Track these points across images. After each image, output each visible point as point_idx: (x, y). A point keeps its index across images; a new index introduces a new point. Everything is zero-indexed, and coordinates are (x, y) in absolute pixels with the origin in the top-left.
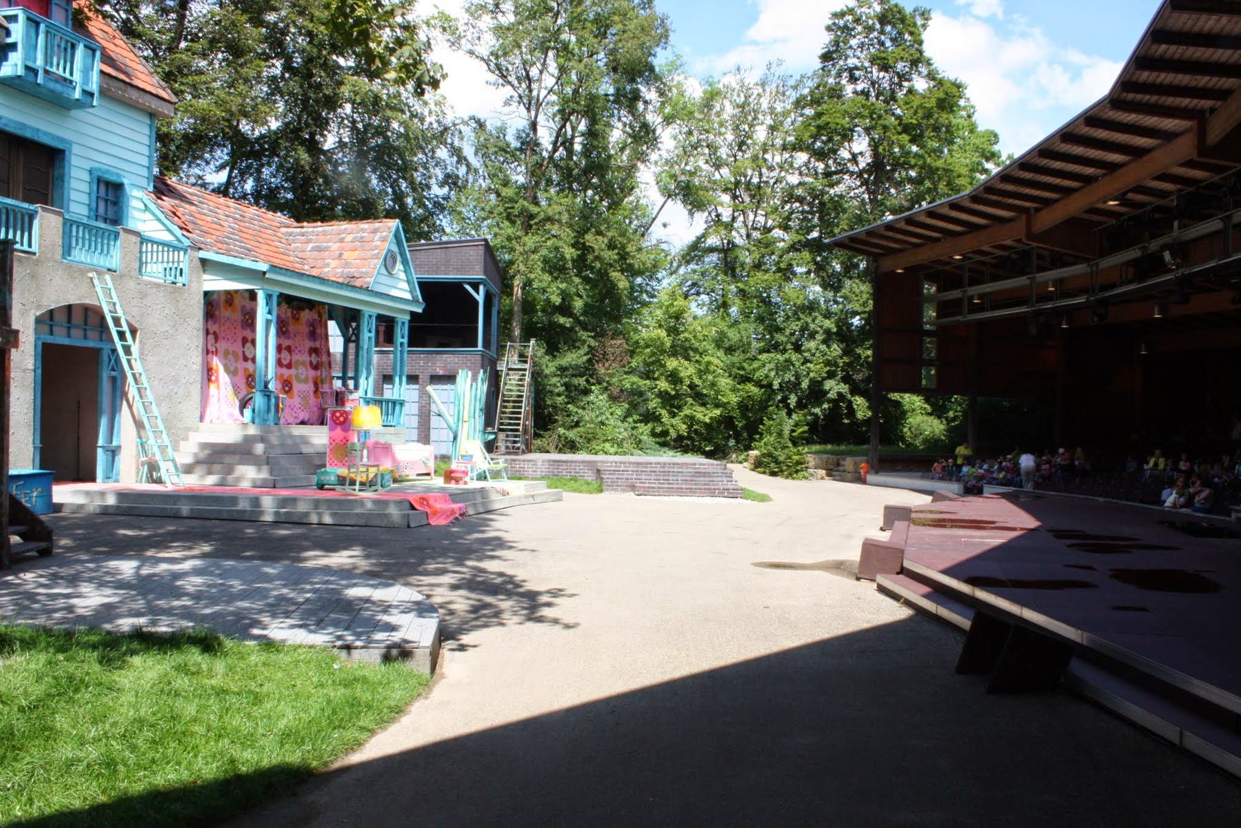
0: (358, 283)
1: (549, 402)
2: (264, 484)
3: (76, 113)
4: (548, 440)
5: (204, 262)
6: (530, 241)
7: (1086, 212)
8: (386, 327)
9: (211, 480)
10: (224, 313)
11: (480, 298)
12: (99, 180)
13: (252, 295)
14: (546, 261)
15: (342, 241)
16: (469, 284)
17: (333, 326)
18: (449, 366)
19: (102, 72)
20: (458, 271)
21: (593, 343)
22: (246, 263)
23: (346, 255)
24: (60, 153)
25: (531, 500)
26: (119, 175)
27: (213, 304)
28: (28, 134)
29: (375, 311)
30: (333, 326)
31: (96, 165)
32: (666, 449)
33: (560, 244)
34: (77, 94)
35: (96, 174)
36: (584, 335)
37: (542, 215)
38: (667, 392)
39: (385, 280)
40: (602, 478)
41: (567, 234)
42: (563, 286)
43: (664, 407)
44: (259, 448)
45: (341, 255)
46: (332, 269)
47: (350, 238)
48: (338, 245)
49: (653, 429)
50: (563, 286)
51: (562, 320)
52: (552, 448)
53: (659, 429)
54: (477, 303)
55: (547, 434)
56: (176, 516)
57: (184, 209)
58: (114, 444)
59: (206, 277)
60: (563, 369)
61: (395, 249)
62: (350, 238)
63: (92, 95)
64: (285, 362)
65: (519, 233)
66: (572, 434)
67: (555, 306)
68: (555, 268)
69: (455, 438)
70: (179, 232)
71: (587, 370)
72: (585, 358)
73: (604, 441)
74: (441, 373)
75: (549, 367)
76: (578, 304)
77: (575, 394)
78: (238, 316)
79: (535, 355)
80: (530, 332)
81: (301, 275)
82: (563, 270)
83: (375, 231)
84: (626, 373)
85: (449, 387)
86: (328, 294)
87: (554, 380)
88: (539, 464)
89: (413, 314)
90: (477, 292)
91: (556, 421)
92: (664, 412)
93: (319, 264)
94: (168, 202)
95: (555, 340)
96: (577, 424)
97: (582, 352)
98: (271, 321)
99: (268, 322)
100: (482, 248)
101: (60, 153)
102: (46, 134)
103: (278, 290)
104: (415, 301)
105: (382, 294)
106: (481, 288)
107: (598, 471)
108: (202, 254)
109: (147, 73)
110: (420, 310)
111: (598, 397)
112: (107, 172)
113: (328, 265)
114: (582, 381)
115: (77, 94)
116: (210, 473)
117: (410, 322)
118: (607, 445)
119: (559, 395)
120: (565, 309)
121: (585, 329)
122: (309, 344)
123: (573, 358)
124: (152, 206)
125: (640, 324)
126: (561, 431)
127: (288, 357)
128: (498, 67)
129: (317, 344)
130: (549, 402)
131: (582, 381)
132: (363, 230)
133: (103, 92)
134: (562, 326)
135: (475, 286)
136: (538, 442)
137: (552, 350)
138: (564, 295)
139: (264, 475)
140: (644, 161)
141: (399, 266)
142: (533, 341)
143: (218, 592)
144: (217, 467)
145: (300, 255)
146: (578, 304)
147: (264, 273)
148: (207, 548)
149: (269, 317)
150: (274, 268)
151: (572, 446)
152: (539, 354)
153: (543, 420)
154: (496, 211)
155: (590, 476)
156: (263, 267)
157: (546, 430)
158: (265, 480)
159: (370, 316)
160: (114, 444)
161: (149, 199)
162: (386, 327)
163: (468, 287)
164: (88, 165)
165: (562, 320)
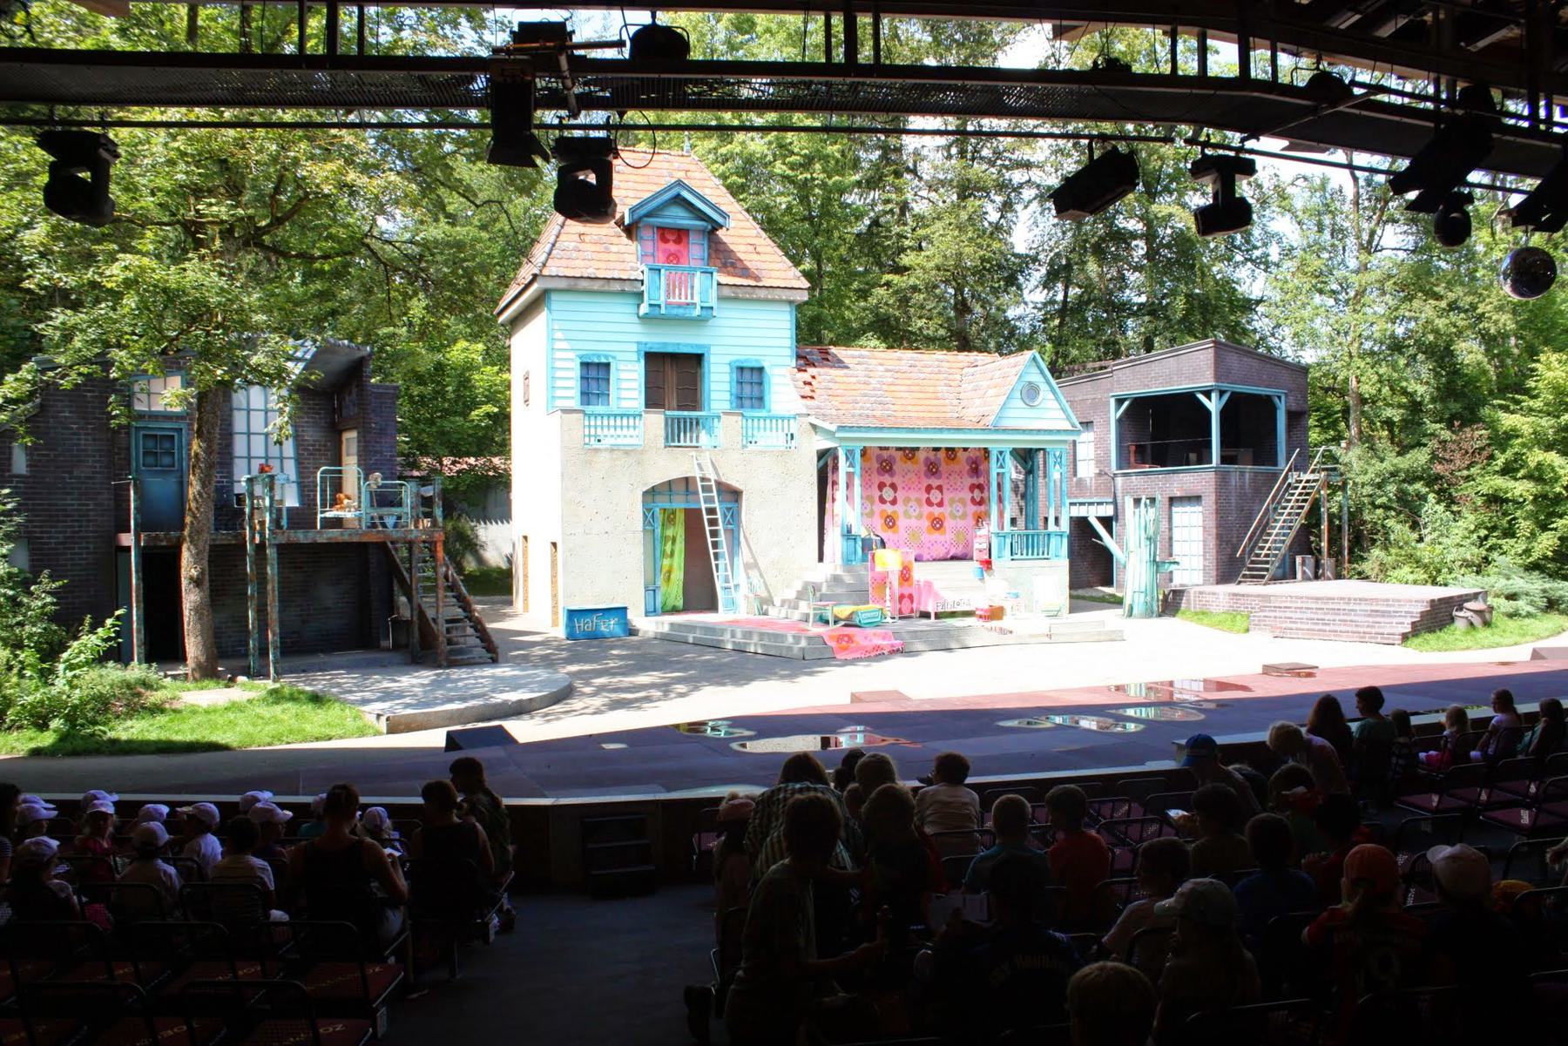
5: (814, 427)
7: (819, 461)
12: (741, 369)
18: (1185, 487)
20: (1192, 380)
26: (757, 361)
28: (670, 350)
29: (1008, 447)
34: (697, 312)
54: (1208, 413)
64: (935, 501)
98: (853, 473)
102: (686, 345)
105: (1039, 430)
112: (746, 361)
122: (969, 481)
125: (1425, 435)
127: (940, 496)
128: (390, 243)
129: (981, 480)
133: (721, 298)
135: (1207, 394)
140: (1399, 183)
148: (259, 805)
149: (851, 470)
156: (833, 428)
159: (1001, 453)
164: (728, 359)
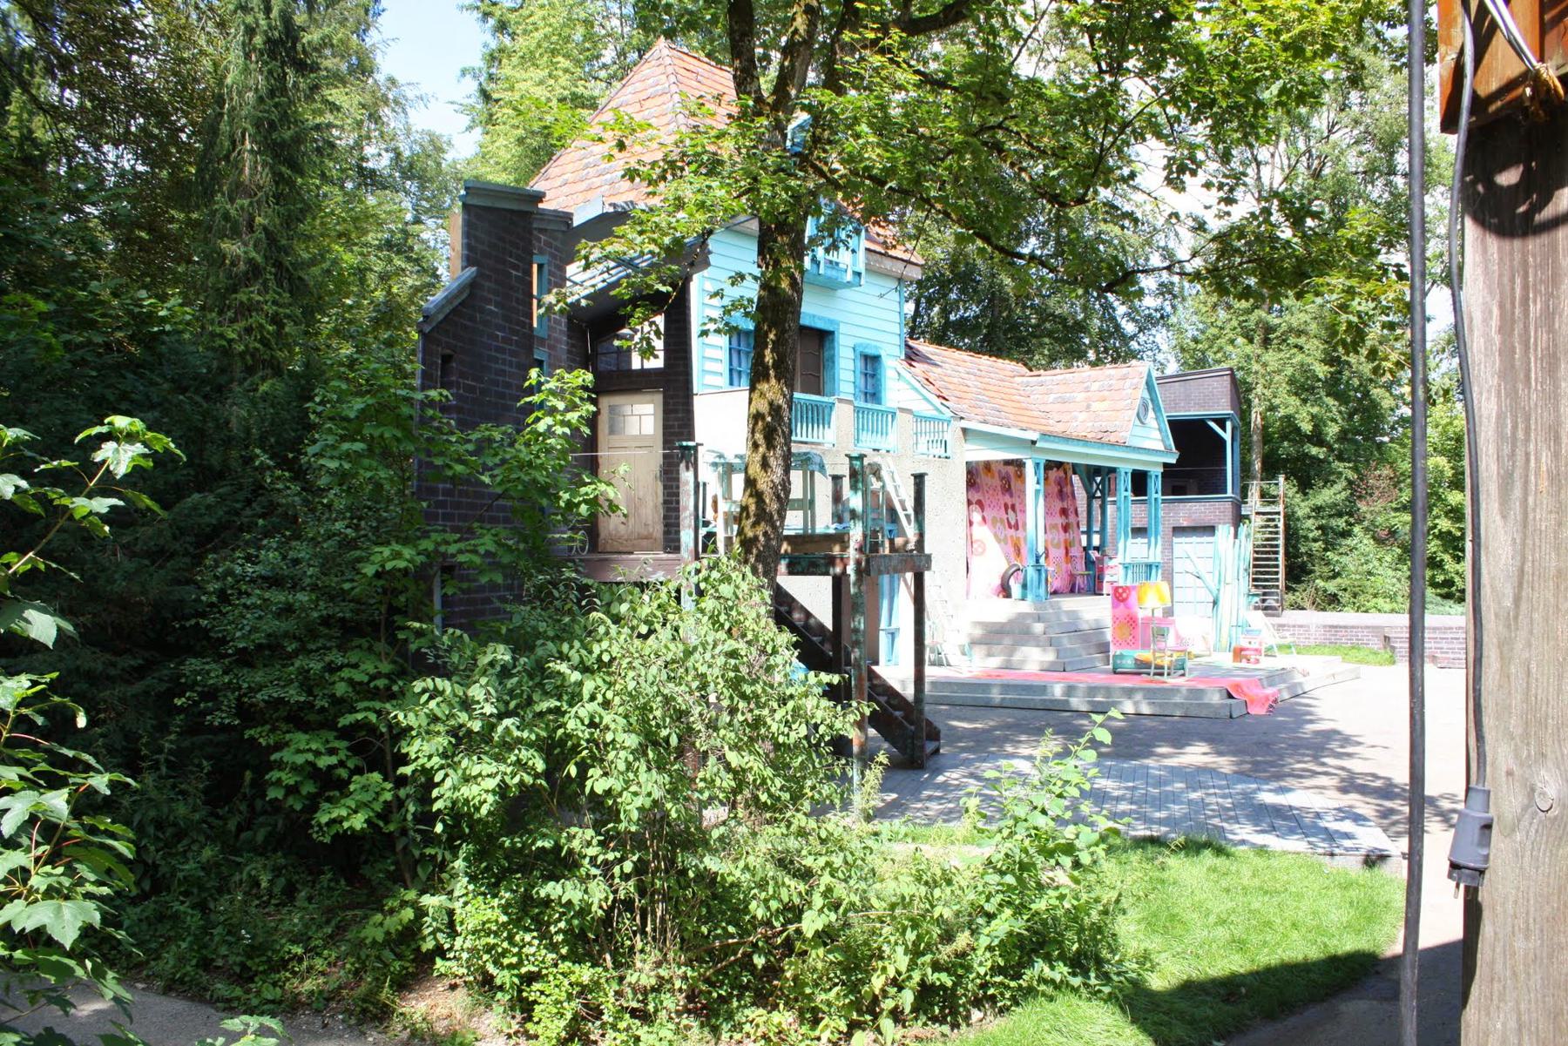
0: (1113, 438)
1: (1303, 550)
2: (1050, 668)
3: (844, 293)
4: (1303, 594)
5: (965, 431)
6: (1271, 357)
8: (1139, 482)
9: (995, 662)
10: (984, 479)
11: (1227, 436)
13: (1019, 464)
14: (1291, 381)
15: (1087, 390)
16: (1215, 420)
17: (1076, 479)
19: (868, 250)
21: (1352, 475)
22: (1014, 433)
23: (1096, 406)
24: (831, 333)
25: (1331, 680)
27: (975, 476)
29: (1129, 468)
30: (1076, 479)
31: (860, 341)
32: (1451, 602)
33: (1309, 360)
34: (849, 277)
35: (860, 349)
36: (1339, 466)
37: (1284, 327)
38: (1449, 533)
39: (1139, 431)
40: (1393, 648)
41: (1315, 348)
42: (1315, 410)
43: (1445, 551)
44: (1038, 628)
45: (1088, 407)
46: (1080, 424)
47: (1095, 386)
48: (1083, 395)
49: (1433, 576)
50: (1315, 410)
51: (1314, 451)
52: (1307, 604)
53: (1440, 578)
54: (1223, 442)
55: (1300, 587)
56: (988, 706)
57: (934, 373)
58: (894, 626)
59: (969, 446)
60: (1318, 509)
61: (1147, 396)
62: (1095, 386)
63: (859, 274)
65: (1259, 351)
66: (1331, 586)
67: (1306, 435)
68: (1303, 387)
69: (1215, 603)
70: (937, 402)
71: (1348, 511)
72: (1344, 495)
73: (1375, 596)
74: (1185, 524)
75: (1303, 509)
76: (1332, 430)
77: (1333, 538)
78: (997, 482)
79: (1285, 495)
80: (1272, 467)
81: (1068, 439)
82: (1312, 389)
83: (1124, 378)
84: (1396, 510)
85: (1206, 539)
86: (1087, 455)
87: (1310, 523)
88: (1313, 630)
89: (1165, 465)
90: (1224, 429)
91: (1312, 572)
92: (1447, 557)
93: (1064, 417)
94: (920, 367)
95: (1306, 475)
96: (1336, 575)
97: (1338, 487)
99: (1037, 492)
100: (1228, 379)
101: (831, 333)
102: (820, 318)
103: (1042, 458)
104: (1168, 451)
106: (1229, 425)
107: (1387, 638)
108: (964, 424)
109: (653, 121)
110: (1174, 461)
111: (1361, 540)
113: (1075, 419)
114: (1340, 523)
115: (849, 277)
116: (989, 655)
117: (1164, 475)
118: (1380, 601)
119: (1315, 540)
120: (1317, 438)
121: (1340, 458)
123: (1327, 495)
124: (904, 373)
126: (1320, 583)
130: (1303, 550)
131: (1340, 523)
132: (1110, 377)
133: (870, 270)
134: (1314, 459)
135: (1222, 425)
136: (1290, 597)
137: (1305, 486)
138: (1318, 422)
139: (1050, 656)
141: (1151, 414)
142: (1281, 479)
143: (112, 517)
144: (996, 649)
145: (1043, 408)
146: (1332, 430)
147: (1034, 442)
150: (1045, 436)
151: (1332, 601)
152: (1290, 494)
153: (1297, 573)
154: (1228, 326)
155: (1376, 644)
156: (1034, 436)
157: (1299, 581)
158: (1052, 663)
160: (894, 626)
161: (902, 366)
162: (1139, 482)
163: (1213, 425)
165: (1314, 451)
